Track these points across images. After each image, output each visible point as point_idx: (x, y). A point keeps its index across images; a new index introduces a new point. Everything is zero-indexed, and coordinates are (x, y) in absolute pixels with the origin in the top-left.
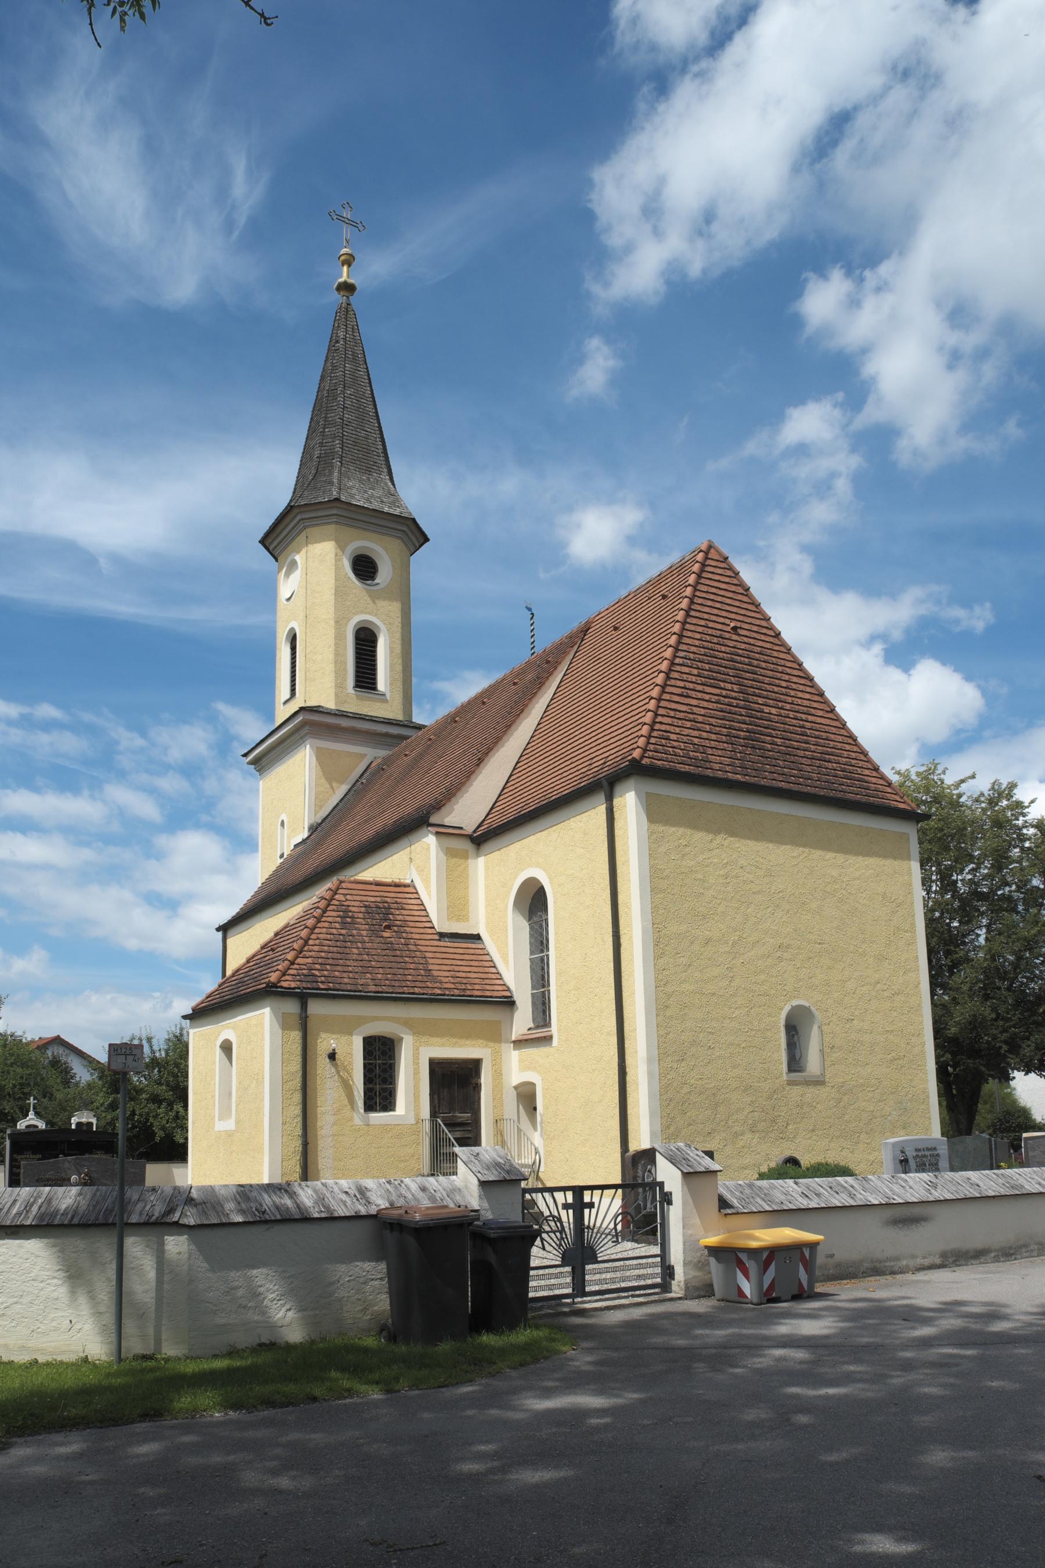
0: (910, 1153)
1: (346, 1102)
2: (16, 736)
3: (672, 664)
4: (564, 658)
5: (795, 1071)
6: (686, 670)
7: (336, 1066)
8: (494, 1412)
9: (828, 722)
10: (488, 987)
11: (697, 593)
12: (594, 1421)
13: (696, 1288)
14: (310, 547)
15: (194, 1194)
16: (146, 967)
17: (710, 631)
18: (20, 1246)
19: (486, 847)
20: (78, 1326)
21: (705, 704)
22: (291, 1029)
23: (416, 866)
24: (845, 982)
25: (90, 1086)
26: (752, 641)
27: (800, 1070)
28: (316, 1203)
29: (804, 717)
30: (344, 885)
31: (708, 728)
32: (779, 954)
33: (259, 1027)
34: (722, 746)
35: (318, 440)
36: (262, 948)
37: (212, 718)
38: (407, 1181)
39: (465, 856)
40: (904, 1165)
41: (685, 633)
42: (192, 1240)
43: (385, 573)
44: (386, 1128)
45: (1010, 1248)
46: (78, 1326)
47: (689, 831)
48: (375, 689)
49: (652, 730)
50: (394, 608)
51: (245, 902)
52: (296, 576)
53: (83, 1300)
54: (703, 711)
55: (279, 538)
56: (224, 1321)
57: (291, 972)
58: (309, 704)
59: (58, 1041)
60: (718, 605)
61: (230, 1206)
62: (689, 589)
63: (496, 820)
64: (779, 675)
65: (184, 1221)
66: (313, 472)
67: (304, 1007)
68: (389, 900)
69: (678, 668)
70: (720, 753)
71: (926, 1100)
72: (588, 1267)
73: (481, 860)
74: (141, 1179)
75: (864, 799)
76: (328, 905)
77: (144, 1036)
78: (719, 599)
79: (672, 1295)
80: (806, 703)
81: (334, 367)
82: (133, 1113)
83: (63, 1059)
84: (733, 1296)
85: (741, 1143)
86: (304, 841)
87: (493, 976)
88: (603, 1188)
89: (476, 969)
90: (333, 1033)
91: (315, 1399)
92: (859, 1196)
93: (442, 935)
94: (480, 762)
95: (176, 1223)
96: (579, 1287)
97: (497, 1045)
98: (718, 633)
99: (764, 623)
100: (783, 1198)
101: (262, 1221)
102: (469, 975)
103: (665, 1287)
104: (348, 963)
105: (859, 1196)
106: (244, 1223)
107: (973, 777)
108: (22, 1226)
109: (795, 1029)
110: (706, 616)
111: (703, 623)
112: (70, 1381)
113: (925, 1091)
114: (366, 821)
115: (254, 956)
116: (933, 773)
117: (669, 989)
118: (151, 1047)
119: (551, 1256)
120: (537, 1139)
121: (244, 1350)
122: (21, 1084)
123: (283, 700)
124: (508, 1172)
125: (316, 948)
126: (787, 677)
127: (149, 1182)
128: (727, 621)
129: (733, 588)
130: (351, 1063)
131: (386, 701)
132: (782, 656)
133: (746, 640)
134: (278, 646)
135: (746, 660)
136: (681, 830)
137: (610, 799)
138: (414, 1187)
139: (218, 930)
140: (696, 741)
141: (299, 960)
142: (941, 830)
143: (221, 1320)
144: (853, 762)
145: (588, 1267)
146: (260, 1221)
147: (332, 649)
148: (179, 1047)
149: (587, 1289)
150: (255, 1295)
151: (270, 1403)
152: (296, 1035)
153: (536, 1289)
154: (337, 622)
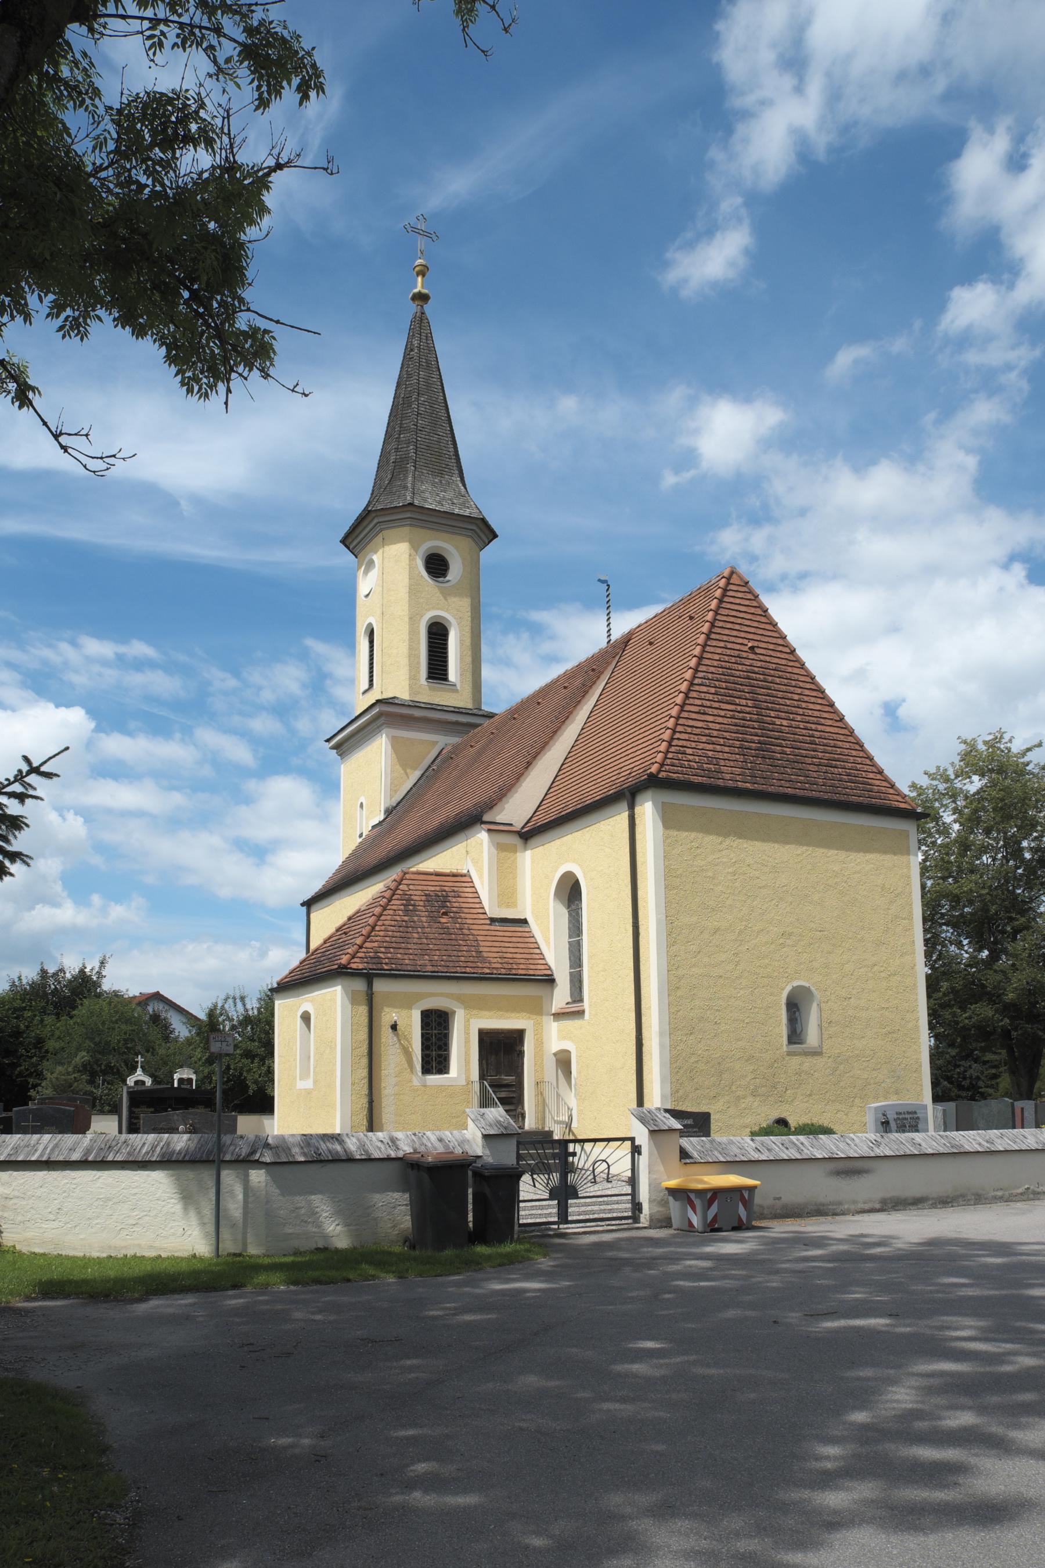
0: (891, 1116)
1: (406, 1066)
2: (111, 675)
3: (692, 684)
4: (606, 668)
5: (795, 1043)
6: (704, 689)
7: (397, 1035)
8: (467, 1289)
9: (836, 730)
10: (532, 967)
11: (718, 617)
12: (528, 1294)
13: (659, 1221)
14: (387, 548)
15: (270, 1141)
16: (239, 916)
17: (729, 652)
18: (148, 1176)
19: (533, 842)
20: (189, 1233)
21: (720, 720)
22: (359, 1004)
23: (470, 857)
24: (843, 965)
25: (189, 1042)
26: (768, 659)
27: (800, 1042)
28: (358, 1148)
29: (814, 726)
30: (407, 876)
31: (722, 741)
32: (782, 941)
33: (332, 1001)
34: (734, 757)
35: (394, 445)
36: (337, 930)
37: (304, 656)
38: (428, 1133)
39: (514, 850)
40: (885, 1125)
41: (705, 655)
42: (268, 1173)
43: (456, 571)
44: (441, 1088)
45: (948, 1197)
46: (189, 1233)
47: (700, 835)
48: (446, 679)
49: (670, 745)
50: (464, 604)
51: (331, 875)
52: (374, 573)
53: (192, 1214)
54: (718, 727)
55: (358, 537)
56: (290, 1231)
57: (359, 955)
58: (385, 696)
59: (157, 996)
60: (737, 627)
61: (296, 1150)
62: (711, 614)
63: (543, 819)
64: (792, 689)
65: (263, 1159)
66: (389, 476)
67: (370, 985)
68: (446, 889)
69: (697, 688)
70: (732, 764)
71: (918, 1070)
72: (570, 1201)
73: (528, 853)
74: (233, 1129)
75: (866, 801)
76: (393, 895)
77: (238, 996)
78: (739, 621)
79: (640, 1225)
80: (816, 714)
81: (409, 376)
82: (228, 1068)
83: (163, 1015)
84: (686, 1227)
85: (743, 1106)
86: (381, 823)
87: (537, 957)
88: (595, 1141)
89: (521, 951)
90: (395, 1007)
91: (349, 1280)
92: (806, 1151)
93: (493, 920)
94: (529, 764)
95: (257, 1161)
96: (563, 1216)
97: (538, 1018)
98: (736, 653)
99: (780, 641)
100: (737, 1151)
101: (317, 1161)
102: (515, 956)
103: (635, 1218)
104: (409, 946)
105: (806, 1151)
106: (305, 1162)
107: (1040, 745)
108: (150, 1162)
109: (795, 1007)
110: (725, 638)
111: (722, 644)
112: (184, 1267)
113: (918, 1062)
114: (433, 810)
115: (330, 938)
116: (1000, 742)
117: (681, 972)
118: (244, 1005)
119: (540, 1192)
120: (572, 1101)
121: (305, 1252)
122: (125, 1040)
123: (362, 690)
124: (506, 1128)
125: (382, 933)
126: (799, 691)
127: (240, 1131)
128: (745, 642)
129: (752, 610)
130: (410, 1033)
131: (457, 691)
132: (796, 671)
133: (762, 658)
134: (357, 639)
135: (762, 677)
136: (693, 835)
137: (632, 807)
138: (433, 1138)
139: (302, 905)
140: (710, 754)
141: (367, 945)
142: (1002, 800)
143: (289, 1230)
144: (859, 766)
145: (570, 1201)
146: (320, 1161)
147: (407, 643)
148: (260, 1030)
149: (570, 1218)
150: (313, 1213)
151: (317, 1281)
152: (363, 1010)
153: (526, 1216)
154: (410, 618)
